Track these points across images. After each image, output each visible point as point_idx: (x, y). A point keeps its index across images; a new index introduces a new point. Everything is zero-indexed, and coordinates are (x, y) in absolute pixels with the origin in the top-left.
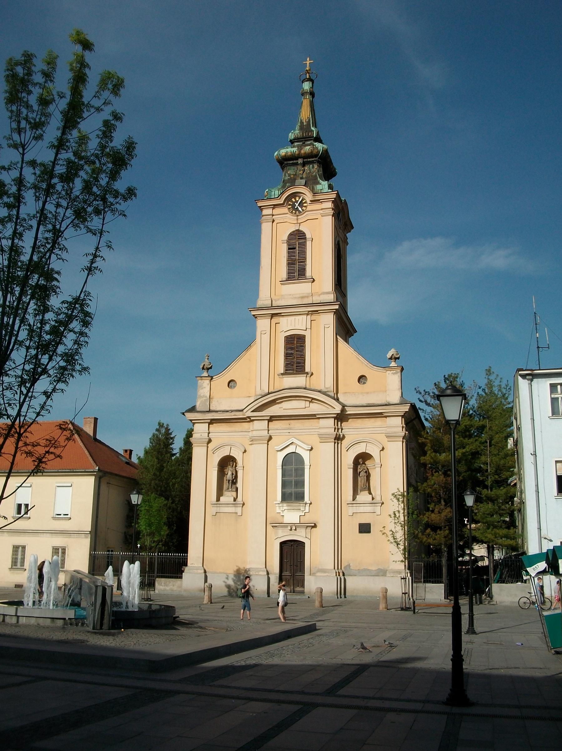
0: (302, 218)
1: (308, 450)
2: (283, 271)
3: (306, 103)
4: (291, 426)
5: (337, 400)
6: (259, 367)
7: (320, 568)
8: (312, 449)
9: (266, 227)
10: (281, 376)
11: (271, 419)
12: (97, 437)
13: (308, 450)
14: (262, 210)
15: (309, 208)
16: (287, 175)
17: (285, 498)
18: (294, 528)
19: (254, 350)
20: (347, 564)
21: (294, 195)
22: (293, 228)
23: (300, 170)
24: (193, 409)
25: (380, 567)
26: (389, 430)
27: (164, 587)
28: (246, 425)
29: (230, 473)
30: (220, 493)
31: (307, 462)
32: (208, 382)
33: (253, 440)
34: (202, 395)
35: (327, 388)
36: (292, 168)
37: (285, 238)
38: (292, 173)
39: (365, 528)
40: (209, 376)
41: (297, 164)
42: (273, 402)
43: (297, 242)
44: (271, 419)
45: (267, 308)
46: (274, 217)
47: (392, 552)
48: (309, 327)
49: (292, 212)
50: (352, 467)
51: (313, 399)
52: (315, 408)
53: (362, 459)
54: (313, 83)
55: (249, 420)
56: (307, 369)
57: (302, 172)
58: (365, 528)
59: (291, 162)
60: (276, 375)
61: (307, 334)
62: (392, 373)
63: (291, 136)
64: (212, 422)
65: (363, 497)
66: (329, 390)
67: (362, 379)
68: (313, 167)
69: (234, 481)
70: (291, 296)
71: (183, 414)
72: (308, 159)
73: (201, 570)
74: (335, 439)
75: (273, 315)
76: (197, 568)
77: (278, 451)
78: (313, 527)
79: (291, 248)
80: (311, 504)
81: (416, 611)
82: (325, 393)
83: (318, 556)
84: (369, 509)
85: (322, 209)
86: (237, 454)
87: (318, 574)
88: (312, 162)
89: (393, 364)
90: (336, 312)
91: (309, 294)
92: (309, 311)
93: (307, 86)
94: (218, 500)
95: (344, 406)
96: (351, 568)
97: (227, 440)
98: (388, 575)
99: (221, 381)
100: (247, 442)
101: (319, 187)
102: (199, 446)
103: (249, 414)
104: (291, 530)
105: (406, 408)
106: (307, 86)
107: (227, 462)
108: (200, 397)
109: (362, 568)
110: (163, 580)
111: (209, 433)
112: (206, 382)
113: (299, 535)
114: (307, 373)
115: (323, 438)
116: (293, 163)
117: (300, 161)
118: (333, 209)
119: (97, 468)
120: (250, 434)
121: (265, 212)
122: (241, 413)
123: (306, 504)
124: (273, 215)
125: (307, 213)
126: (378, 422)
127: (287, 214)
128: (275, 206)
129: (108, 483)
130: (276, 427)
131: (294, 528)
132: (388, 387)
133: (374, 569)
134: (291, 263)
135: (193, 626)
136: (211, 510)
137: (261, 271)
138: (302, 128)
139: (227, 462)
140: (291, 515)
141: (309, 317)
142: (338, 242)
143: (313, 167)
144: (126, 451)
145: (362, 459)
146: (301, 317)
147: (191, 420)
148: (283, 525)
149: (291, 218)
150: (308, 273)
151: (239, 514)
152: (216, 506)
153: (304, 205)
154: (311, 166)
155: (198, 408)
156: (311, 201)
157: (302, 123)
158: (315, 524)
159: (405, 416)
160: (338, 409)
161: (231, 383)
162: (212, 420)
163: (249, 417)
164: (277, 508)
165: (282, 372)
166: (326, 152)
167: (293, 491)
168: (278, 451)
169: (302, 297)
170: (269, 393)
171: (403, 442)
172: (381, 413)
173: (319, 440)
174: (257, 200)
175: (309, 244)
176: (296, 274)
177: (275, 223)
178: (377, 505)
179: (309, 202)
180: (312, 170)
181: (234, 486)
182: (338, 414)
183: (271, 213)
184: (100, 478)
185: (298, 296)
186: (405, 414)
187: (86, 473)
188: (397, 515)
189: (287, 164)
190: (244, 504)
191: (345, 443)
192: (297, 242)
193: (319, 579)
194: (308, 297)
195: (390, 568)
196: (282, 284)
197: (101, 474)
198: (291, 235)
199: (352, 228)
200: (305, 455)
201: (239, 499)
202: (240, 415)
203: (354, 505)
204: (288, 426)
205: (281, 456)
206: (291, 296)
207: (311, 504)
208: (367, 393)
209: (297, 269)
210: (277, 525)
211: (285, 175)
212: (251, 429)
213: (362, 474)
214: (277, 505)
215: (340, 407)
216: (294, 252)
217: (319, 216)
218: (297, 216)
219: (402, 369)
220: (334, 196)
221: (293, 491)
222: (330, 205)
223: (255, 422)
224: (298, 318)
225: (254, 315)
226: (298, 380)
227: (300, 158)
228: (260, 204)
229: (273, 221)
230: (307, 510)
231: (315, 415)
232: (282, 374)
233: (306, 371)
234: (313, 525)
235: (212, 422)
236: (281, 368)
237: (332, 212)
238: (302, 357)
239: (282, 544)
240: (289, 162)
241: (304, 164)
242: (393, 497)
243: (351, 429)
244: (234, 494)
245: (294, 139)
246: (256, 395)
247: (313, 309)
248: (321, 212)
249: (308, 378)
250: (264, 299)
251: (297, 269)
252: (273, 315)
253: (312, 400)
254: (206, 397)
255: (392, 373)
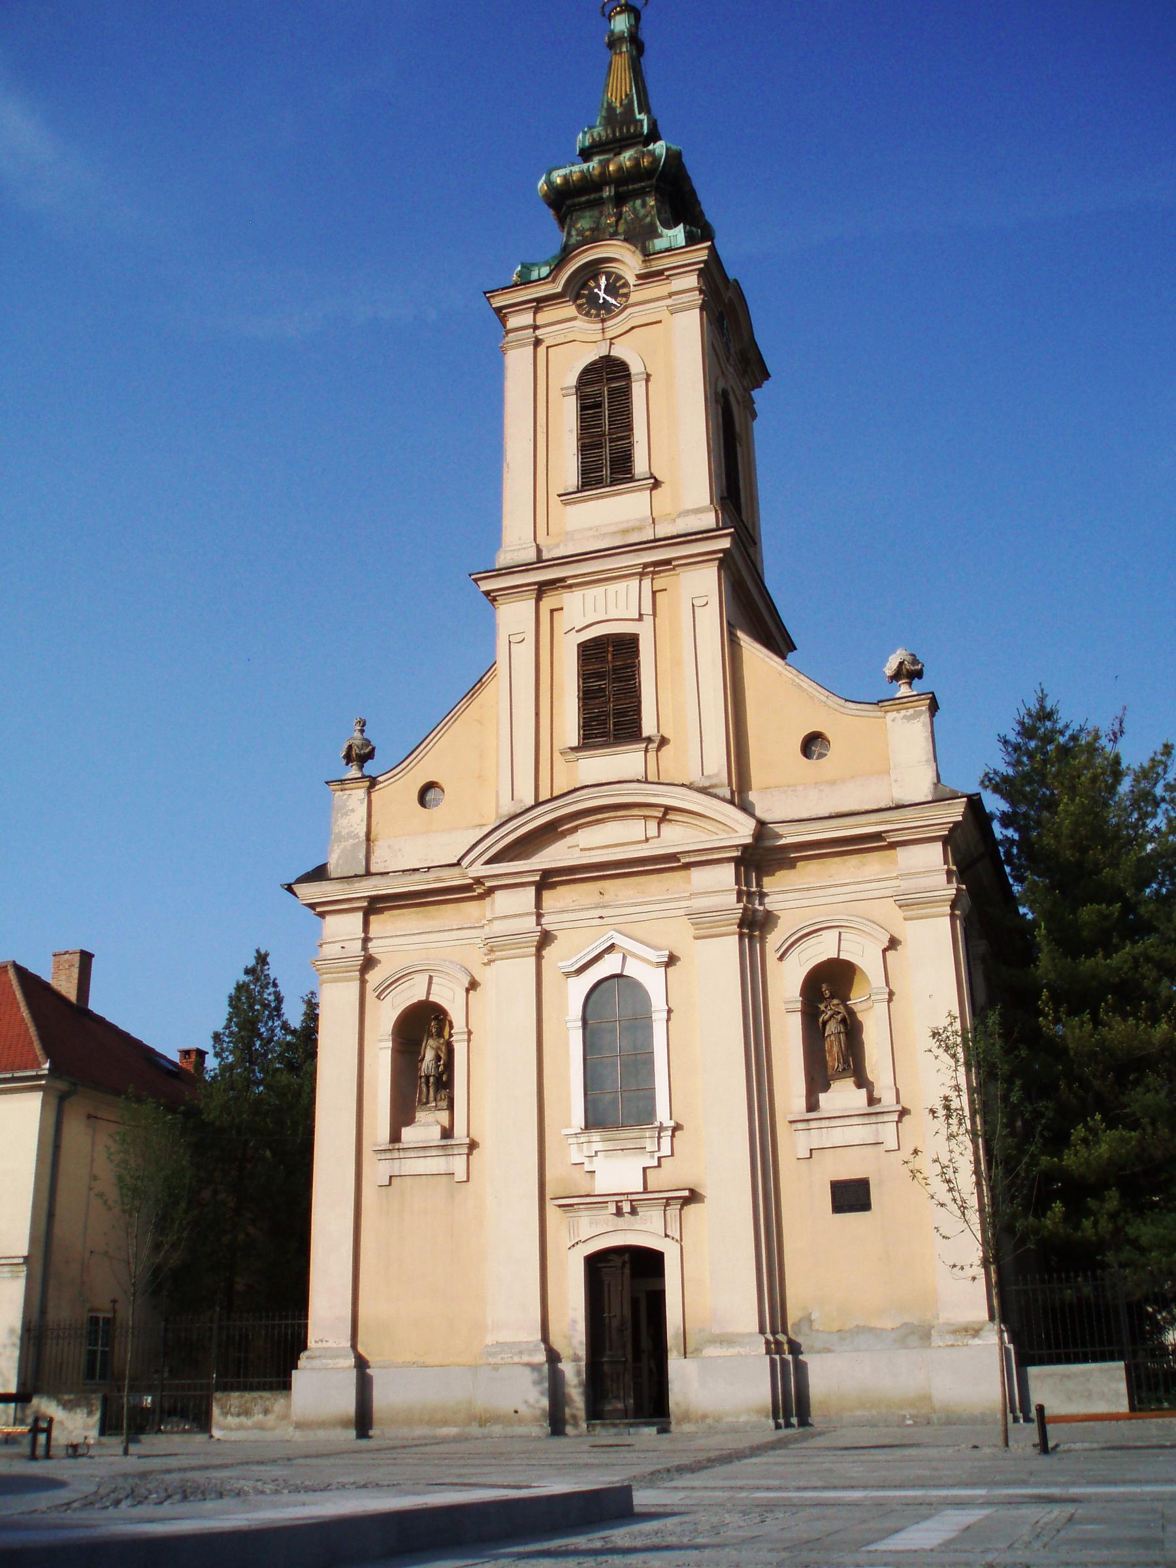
0: (615, 325)
1: (658, 964)
2: (567, 465)
3: (621, 62)
4: (606, 897)
5: (746, 807)
6: (506, 741)
7: (716, 1330)
8: (672, 960)
9: (518, 362)
10: (573, 756)
11: (547, 881)
12: (91, 1006)
13: (658, 964)
14: (503, 320)
15: (633, 298)
16: (574, 233)
17: (596, 1119)
18: (626, 1208)
19: (494, 692)
20: (800, 1314)
21: (593, 269)
22: (591, 355)
23: (609, 216)
24: (319, 874)
25: (907, 1319)
26: (905, 885)
27: (237, 1420)
28: (472, 908)
29: (429, 1055)
30: (402, 1115)
31: (658, 1004)
32: (361, 793)
33: (494, 949)
34: (344, 832)
35: (709, 777)
36: (587, 214)
37: (572, 380)
38: (587, 226)
39: (851, 1196)
40: (364, 777)
41: (599, 203)
42: (550, 832)
43: (605, 392)
44: (547, 881)
45: (526, 568)
46: (538, 332)
47: (943, 1231)
48: (647, 608)
49: (588, 314)
50: (799, 1006)
51: (668, 809)
52: (676, 838)
53: (830, 983)
54: (638, 18)
55: (476, 891)
56: (648, 727)
57: (613, 219)
58: (851, 1196)
59: (583, 199)
60: (556, 755)
61: (644, 631)
62: (905, 717)
63: (582, 140)
64: (374, 906)
65: (843, 1096)
66: (714, 781)
67: (812, 744)
68: (644, 205)
69: (444, 1082)
70: (592, 533)
71: (289, 888)
72: (627, 186)
73: (346, 1357)
74: (740, 926)
75: (542, 589)
76: (335, 1354)
77: (568, 975)
78: (686, 1201)
79: (588, 408)
80: (677, 1128)
81: (1051, 1444)
82: (703, 791)
83: (709, 1289)
84: (859, 1133)
85: (670, 295)
86: (449, 996)
87: (711, 1351)
88: (642, 193)
89: (904, 690)
90: (726, 562)
91: (644, 520)
92: (645, 566)
93: (621, 24)
94: (395, 1137)
95: (761, 824)
96: (816, 1326)
97: (422, 954)
98: (936, 1341)
99: (399, 791)
100: (475, 957)
101: (659, 244)
102: (335, 981)
103: (479, 870)
104: (619, 1212)
105: (955, 812)
106: (621, 24)
107: (422, 1026)
108: (340, 838)
109: (850, 1325)
110: (235, 1399)
111: (366, 940)
112: (359, 793)
113: (644, 1232)
114: (649, 740)
115: (703, 924)
116: (588, 202)
117: (607, 192)
118: (701, 291)
119: (47, 1066)
120: (488, 931)
121: (513, 322)
122: (455, 871)
123: (661, 1128)
124: (536, 327)
125: (629, 311)
126: (871, 866)
127: (574, 319)
128: (539, 304)
129: (89, 1117)
130: (560, 905)
131: (626, 1208)
132: (899, 761)
133: (890, 1325)
134: (588, 445)
135: (83, 1502)
136: (377, 1171)
137: (506, 476)
138: (611, 118)
139: (422, 1026)
140: (617, 1170)
141: (647, 582)
142: (725, 394)
143: (644, 205)
144: (186, 1053)
145: (830, 983)
146: (621, 586)
147: (312, 906)
148: (594, 1201)
149: (585, 327)
150: (640, 466)
151: (461, 1175)
152: (388, 1155)
153: (621, 291)
154: (638, 202)
155: (333, 870)
156: (639, 277)
157: (611, 109)
158: (692, 1191)
159: (951, 840)
160: (742, 830)
161: (427, 793)
162: (374, 900)
163: (478, 881)
164: (574, 1148)
165: (575, 743)
166: (675, 158)
167: (619, 1094)
168: (568, 975)
169: (625, 531)
170: (538, 804)
171: (952, 916)
172: (878, 836)
173: (692, 931)
174: (489, 294)
175: (638, 390)
176: (606, 472)
177: (541, 350)
178: (886, 1118)
179: (632, 281)
180: (642, 212)
181: (443, 1093)
182: (745, 847)
183: (531, 322)
184: (62, 1098)
185: (614, 529)
186: (951, 830)
187: (25, 1085)
188: (955, 1104)
189: (574, 205)
190: (473, 1146)
191: (775, 940)
192: (605, 392)
193: (715, 1378)
194: (640, 529)
195: (941, 1321)
196: (566, 503)
197: (62, 1085)
198: (586, 371)
199: (766, 375)
200: (652, 980)
201: (460, 1130)
202: (454, 878)
203: (813, 1124)
204: (597, 899)
205: (581, 986)
206: (592, 533)
207: (677, 1128)
208: (833, 783)
209: (607, 457)
210: (578, 1202)
211: (569, 234)
212: (489, 916)
213: (831, 1028)
214: (573, 1140)
215: (751, 824)
216: (598, 416)
217: (664, 315)
218: (603, 321)
219: (934, 707)
220: (703, 255)
221: (619, 1094)
222: (692, 281)
223: (498, 894)
224: (612, 587)
225: (487, 593)
226: (620, 763)
227: (607, 184)
228: (498, 302)
229: (537, 342)
230: (666, 1150)
231: (673, 857)
232: (573, 749)
233: (646, 733)
234: (686, 1193)
235: (374, 906)
236: (569, 728)
237: (697, 298)
238: (632, 694)
239: (596, 1264)
240: (577, 200)
241: (620, 200)
242: (933, 1044)
243: (785, 894)
244: (443, 1117)
245: (592, 147)
246: (498, 816)
247: (656, 558)
248: (669, 302)
249: (652, 755)
250: (516, 543)
251: (607, 457)
252: (542, 589)
253: (667, 813)
254: (357, 836)
255: (905, 717)
